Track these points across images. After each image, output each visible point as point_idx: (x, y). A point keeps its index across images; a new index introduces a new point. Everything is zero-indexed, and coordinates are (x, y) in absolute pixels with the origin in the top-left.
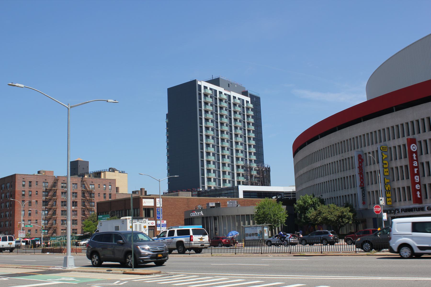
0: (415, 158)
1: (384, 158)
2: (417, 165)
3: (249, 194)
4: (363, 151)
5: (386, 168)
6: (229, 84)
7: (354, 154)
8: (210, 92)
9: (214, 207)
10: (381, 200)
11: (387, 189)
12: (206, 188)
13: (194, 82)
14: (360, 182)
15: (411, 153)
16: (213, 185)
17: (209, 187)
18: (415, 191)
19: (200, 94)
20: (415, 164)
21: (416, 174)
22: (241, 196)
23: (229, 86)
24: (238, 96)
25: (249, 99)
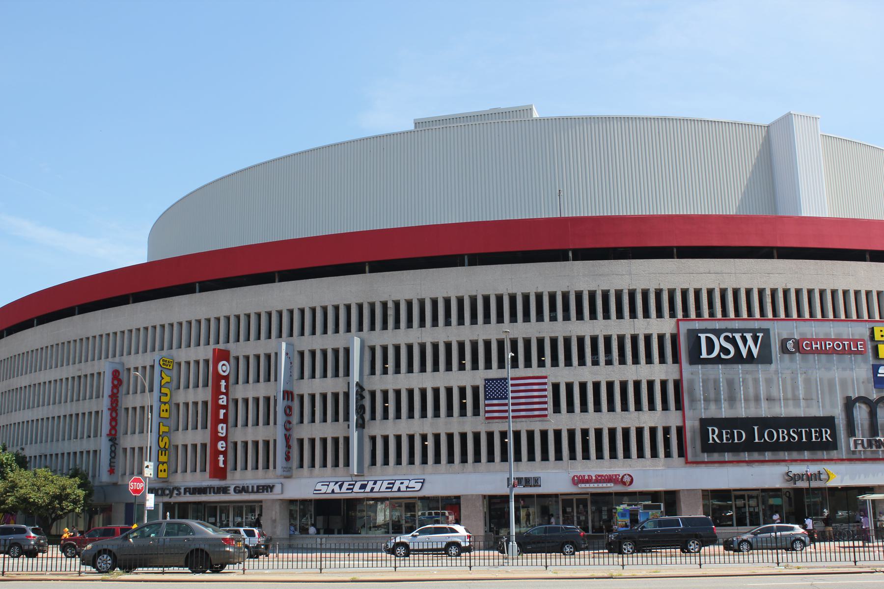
0: (223, 390)
1: (163, 382)
2: (225, 403)
5: (165, 403)
7: (106, 367)
10: (147, 467)
11: (162, 445)
14: (109, 427)
15: (218, 377)
18: (216, 453)
20: (223, 401)
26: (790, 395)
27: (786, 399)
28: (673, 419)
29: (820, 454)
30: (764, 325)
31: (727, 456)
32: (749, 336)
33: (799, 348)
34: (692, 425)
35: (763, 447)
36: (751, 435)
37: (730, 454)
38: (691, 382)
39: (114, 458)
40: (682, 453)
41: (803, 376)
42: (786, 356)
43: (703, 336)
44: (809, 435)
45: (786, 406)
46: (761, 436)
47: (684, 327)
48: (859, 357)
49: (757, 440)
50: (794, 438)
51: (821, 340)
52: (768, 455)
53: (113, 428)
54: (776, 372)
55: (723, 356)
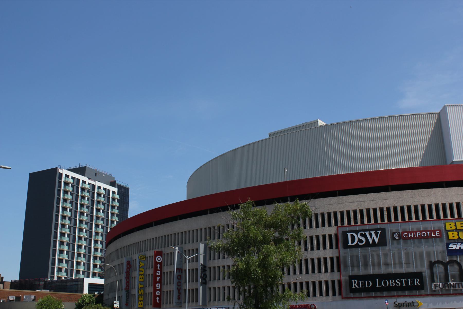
0: (159, 269)
1: (141, 266)
2: (160, 274)
3: (95, 287)
4: (132, 258)
5: (141, 275)
6: (96, 174)
7: (124, 261)
8: (71, 181)
9: (13, 300)
10: (116, 303)
11: (140, 293)
12: (55, 278)
13: (55, 170)
14: (125, 286)
15: (156, 263)
16: (63, 275)
17: (59, 278)
18: (155, 296)
19: (60, 183)
20: (159, 273)
21: (158, 282)
22: (86, 290)
23: (96, 176)
24: (103, 186)
25: (116, 190)
26: (397, 262)
27: (395, 264)
28: (336, 276)
29: (414, 292)
30: (383, 226)
31: (363, 295)
32: (373, 233)
33: (402, 237)
34: (344, 279)
35: (382, 289)
36: (374, 283)
37: (365, 293)
38: (345, 258)
39: (128, 299)
40: (340, 294)
41: (405, 251)
42: (395, 242)
43: (349, 234)
44: (407, 282)
45: (395, 267)
46: (380, 284)
47: (341, 230)
48: (438, 240)
49: (378, 286)
50: (398, 284)
51: (413, 232)
52: (385, 294)
53: (127, 286)
54: (389, 250)
55: (359, 244)
